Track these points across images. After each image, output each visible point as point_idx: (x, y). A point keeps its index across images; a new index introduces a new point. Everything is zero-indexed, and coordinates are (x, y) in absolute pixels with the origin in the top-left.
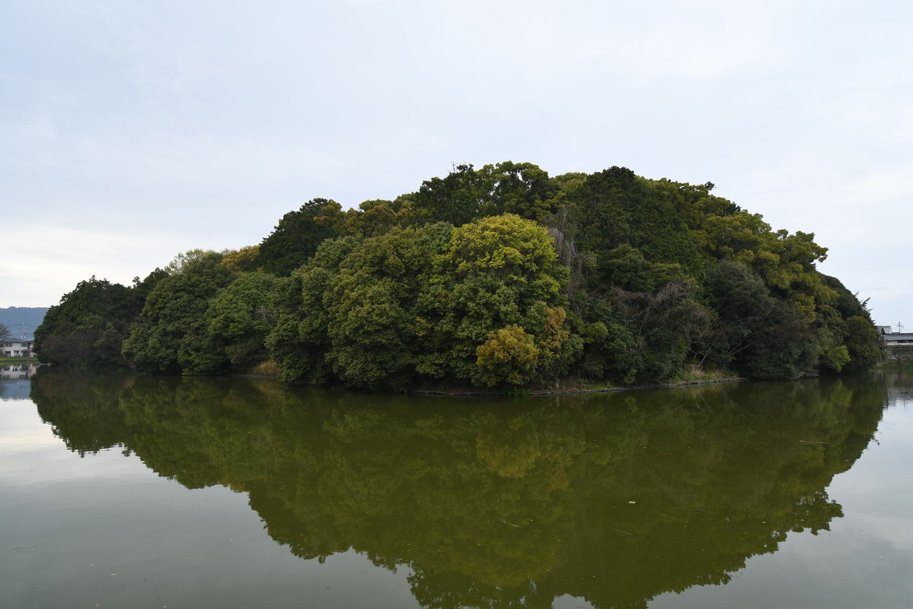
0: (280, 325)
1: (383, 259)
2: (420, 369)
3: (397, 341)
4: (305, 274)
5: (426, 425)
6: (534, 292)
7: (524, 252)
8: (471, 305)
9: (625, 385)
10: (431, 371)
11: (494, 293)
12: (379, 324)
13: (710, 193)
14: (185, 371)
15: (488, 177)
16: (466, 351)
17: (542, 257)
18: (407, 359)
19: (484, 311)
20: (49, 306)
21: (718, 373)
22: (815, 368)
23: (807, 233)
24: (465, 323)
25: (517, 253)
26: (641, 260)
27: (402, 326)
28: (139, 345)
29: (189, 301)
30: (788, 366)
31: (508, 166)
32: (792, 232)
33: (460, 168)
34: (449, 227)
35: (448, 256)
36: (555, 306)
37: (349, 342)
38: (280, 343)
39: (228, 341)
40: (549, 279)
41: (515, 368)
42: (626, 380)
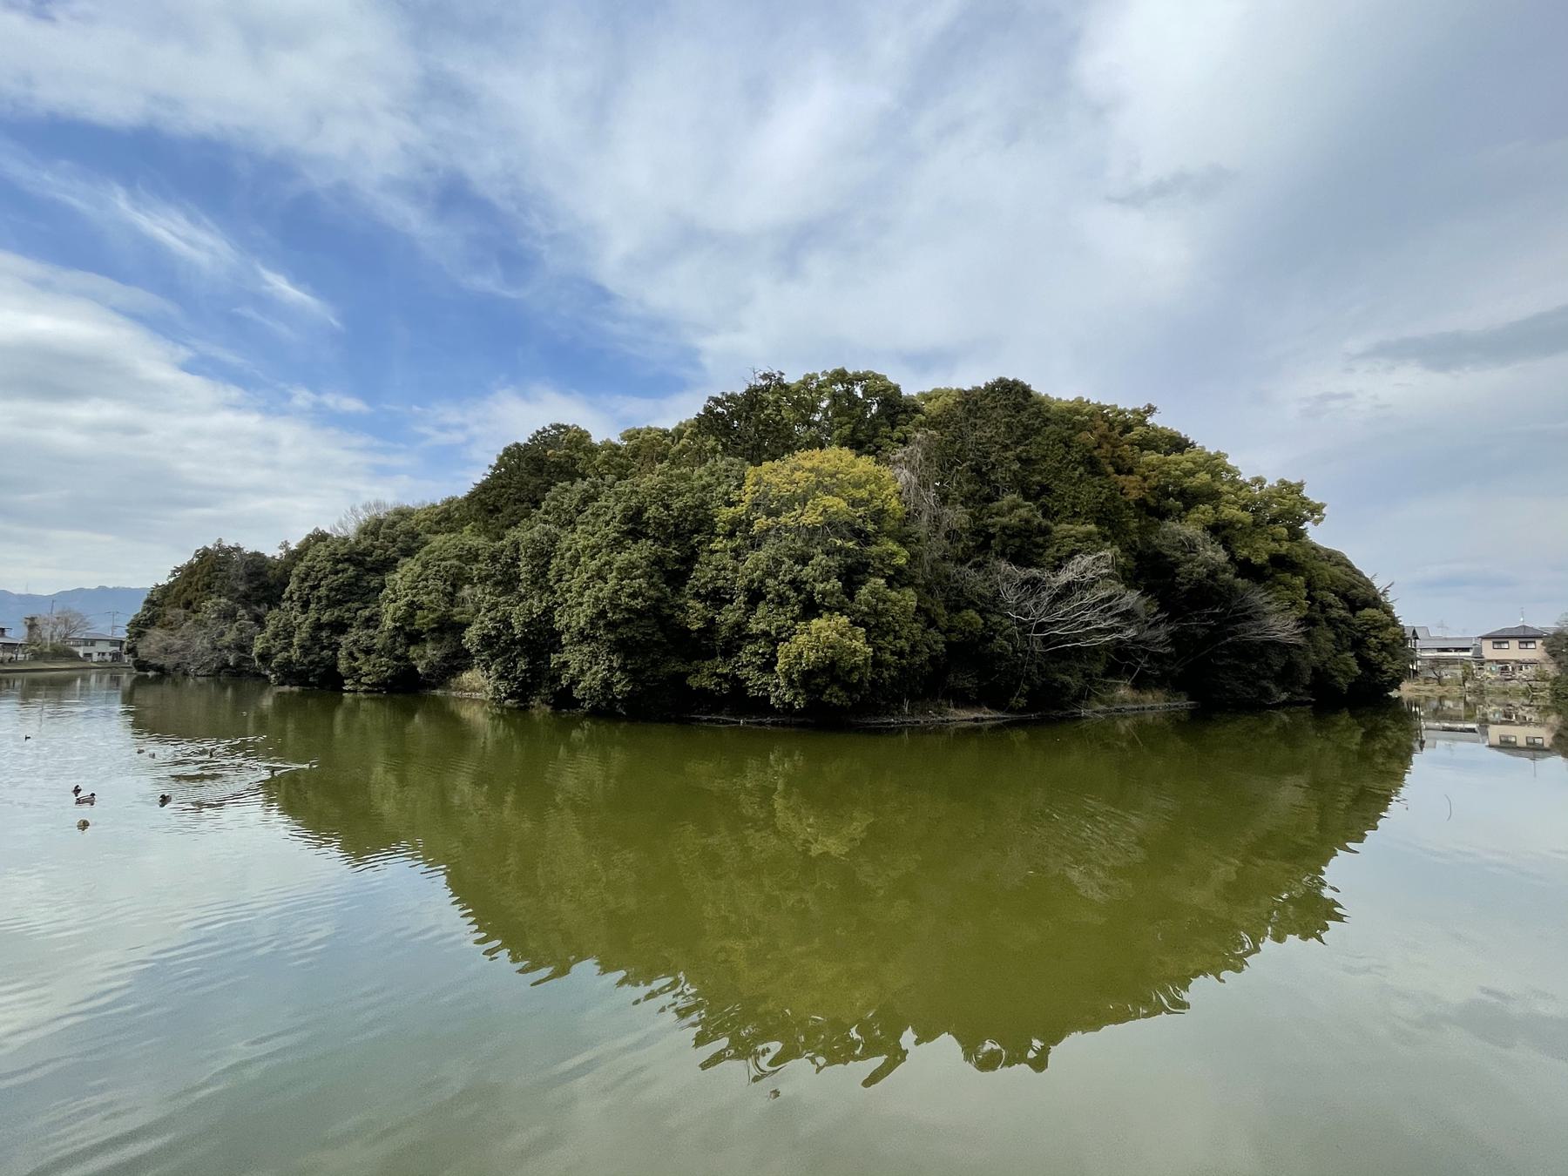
0: (481, 609)
1: (640, 511)
2: (693, 682)
3: (658, 636)
4: (527, 533)
5: (704, 771)
6: (868, 565)
7: (854, 503)
8: (770, 582)
9: (1011, 710)
10: (709, 684)
11: (805, 564)
12: (629, 610)
13: (1150, 421)
14: (348, 685)
15: (810, 392)
16: (763, 654)
17: (882, 511)
18: (676, 666)
19: (792, 594)
20: (150, 585)
21: (1159, 694)
22: (1306, 687)
23: (1293, 482)
24: (762, 609)
25: (844, 504)
26: (1039, 519)
27: (667, 611)
28: (279, 644)
29: (358, 578)
30: (1264, 683)
31: (840, 376)
32: (1271, 482)
33: (765, 377)
34: (743, 466)
35: (741, 509)
36: (902, 586)
37: (583, 637)
38: (487, 641)
39: (415, 638)
40: (892, 546)
41: (835, 679)
42: (1013, 702)
